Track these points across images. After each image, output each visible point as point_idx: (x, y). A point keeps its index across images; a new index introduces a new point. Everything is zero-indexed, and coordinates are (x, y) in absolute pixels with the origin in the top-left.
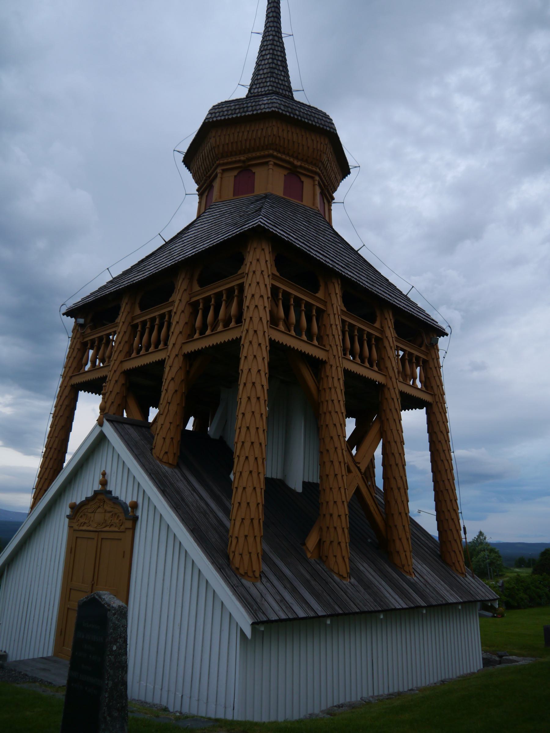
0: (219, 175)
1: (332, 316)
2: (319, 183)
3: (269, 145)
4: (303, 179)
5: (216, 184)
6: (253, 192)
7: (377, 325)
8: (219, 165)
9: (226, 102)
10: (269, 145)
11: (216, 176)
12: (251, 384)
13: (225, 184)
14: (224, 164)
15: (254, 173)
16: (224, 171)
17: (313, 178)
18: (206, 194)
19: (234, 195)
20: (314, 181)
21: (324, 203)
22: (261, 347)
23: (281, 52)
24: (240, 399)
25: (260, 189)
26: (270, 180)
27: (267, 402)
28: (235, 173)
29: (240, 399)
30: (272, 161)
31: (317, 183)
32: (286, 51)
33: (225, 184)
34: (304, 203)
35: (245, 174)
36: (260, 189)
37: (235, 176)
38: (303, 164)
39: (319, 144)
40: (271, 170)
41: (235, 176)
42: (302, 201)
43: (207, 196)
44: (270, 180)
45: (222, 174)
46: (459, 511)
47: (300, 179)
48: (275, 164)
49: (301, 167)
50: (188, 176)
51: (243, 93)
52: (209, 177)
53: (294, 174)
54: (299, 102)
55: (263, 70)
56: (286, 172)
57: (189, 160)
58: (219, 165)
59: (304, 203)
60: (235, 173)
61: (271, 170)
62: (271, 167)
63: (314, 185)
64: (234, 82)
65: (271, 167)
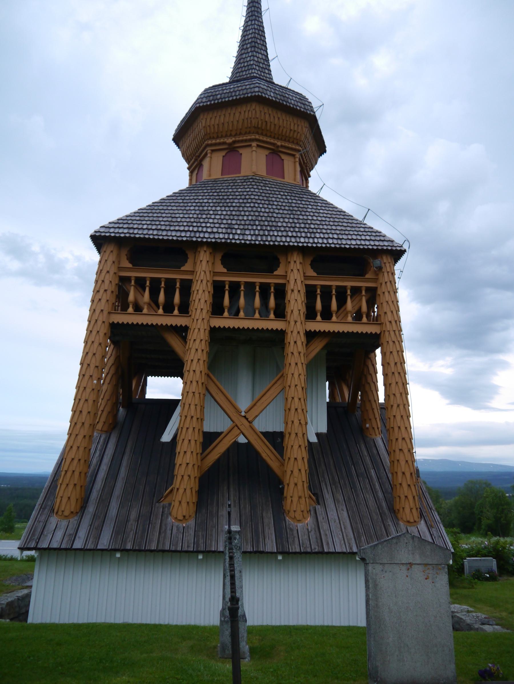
0: (209, 155)
2: (299, 160)
4: (283, 156)
5: (206, 163)
6: (240, 173)
8: (208, 145)
9: (213, 86)
11: (206, 154)
12: (295, 435)
15: (241, 154)
16: (213, 151)
17: (294, 156)
18: (196, 172)
19: (222, 175)
20: (295, 158)
21: (303, 180)
22: (407, 431)
24: (291, 497)
25: (246, 170)
26: (254, 162)
27: (307, 448)
28: (223, 153)
30: (254, 144)
31: (297, 160)
35: (232, 151)
37: (223, 156)
39: (296, 126)
41: (223, 156)
42: (284, 178)
43: (197, 174)
44: (254, 162)
45: (211, 153)
46: (414, 451)
48: (258, 146)
49: (282, 146)
50: (177, 152)
51: (227, 80)
52: (199, 156)
53: (275, 153)
54: (278, 85)
55: (236, 92)
56: (267, 152)
57: (178, 138)
58: (208, 145)
60: (223, 153)
62: (254, 149)
63: (295, 162)
64: (218, 68)
65: (254, 149)
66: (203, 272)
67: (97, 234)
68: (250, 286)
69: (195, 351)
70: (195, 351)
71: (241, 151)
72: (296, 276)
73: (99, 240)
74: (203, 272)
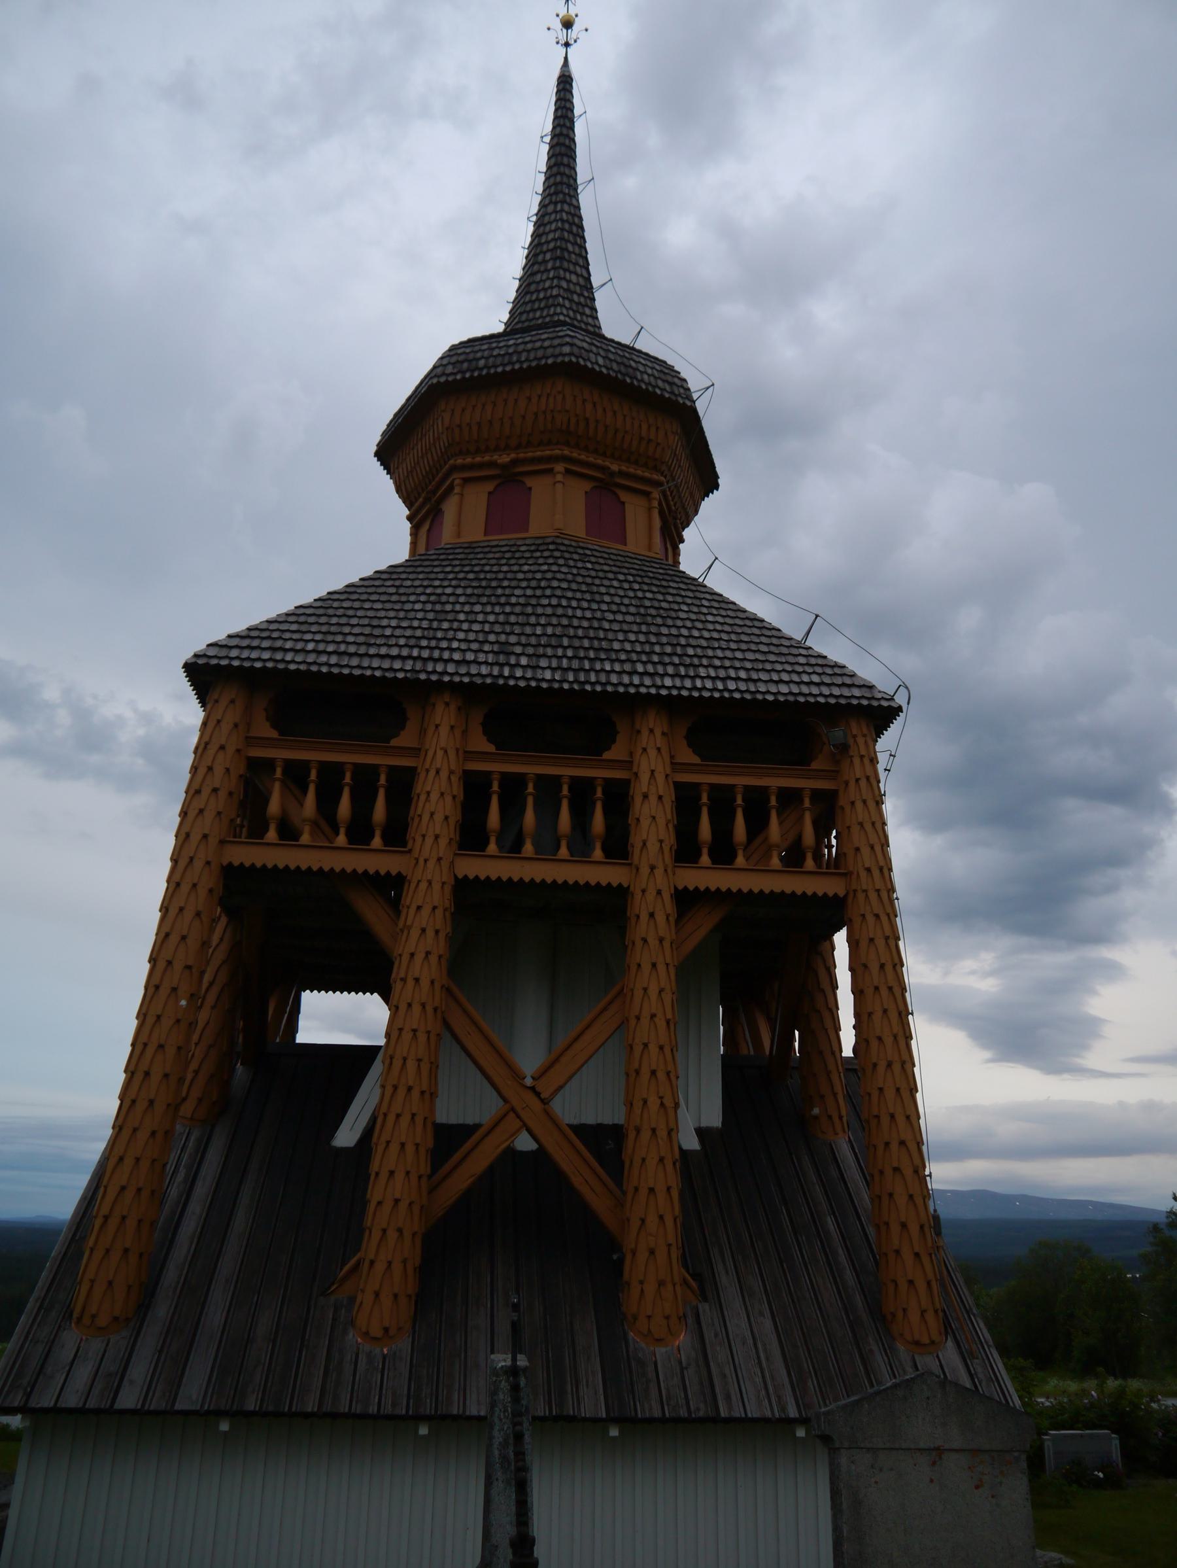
0: (457, 490)
1: (857, 761)
2: (660, 504)
3: (556, 424)
4: (624, 496)
5: (450, 509)
6: (527, 531)
7: (405, 739)
8: (455, 468)
10: (556, 424)
11: (451, 488)
13: (466, 516)
14: (463, 468)
15: (530, 489)
16: (466, 481)
17: (647, 494)
18: (426, 527)
20: (650, 500)
21: (666, 549)
23: (575, 244)
25: (539, 525)
26: (558, 507)
28: (495, 483)
29: (641, 1282)
31: (655, 503)
32: (586, 235)
33: (466, 516)
34: (631, 547)
35: (509, 484)
36: (539, 525)
37: (490, 493)
38: (624, 468)
40: (559, 486)
41: (490, 493)
43: (429, 531)
44: (558, 507)
46: (927, 1173)
47: (618, 498)
48: (568, 472)
49: (622, 474)
52: (434, 492)
53: (606, 491)
54: (612, 341)
56: (587, 486)
58: (455, 468)
59: (631, 547)
60: (490, 486)
61: (559, 486)
62: (559, 477)
63: (650, 509)
64: (479, 301)
65: (559, 477)
66: (441, 750)
67: (200, 661)
68: (548, 786)
69: (420, 934)
70: (420, 934)
71: (530, 482)
72: (653, 764)
73: (204, 674)
74: (441, 750)
